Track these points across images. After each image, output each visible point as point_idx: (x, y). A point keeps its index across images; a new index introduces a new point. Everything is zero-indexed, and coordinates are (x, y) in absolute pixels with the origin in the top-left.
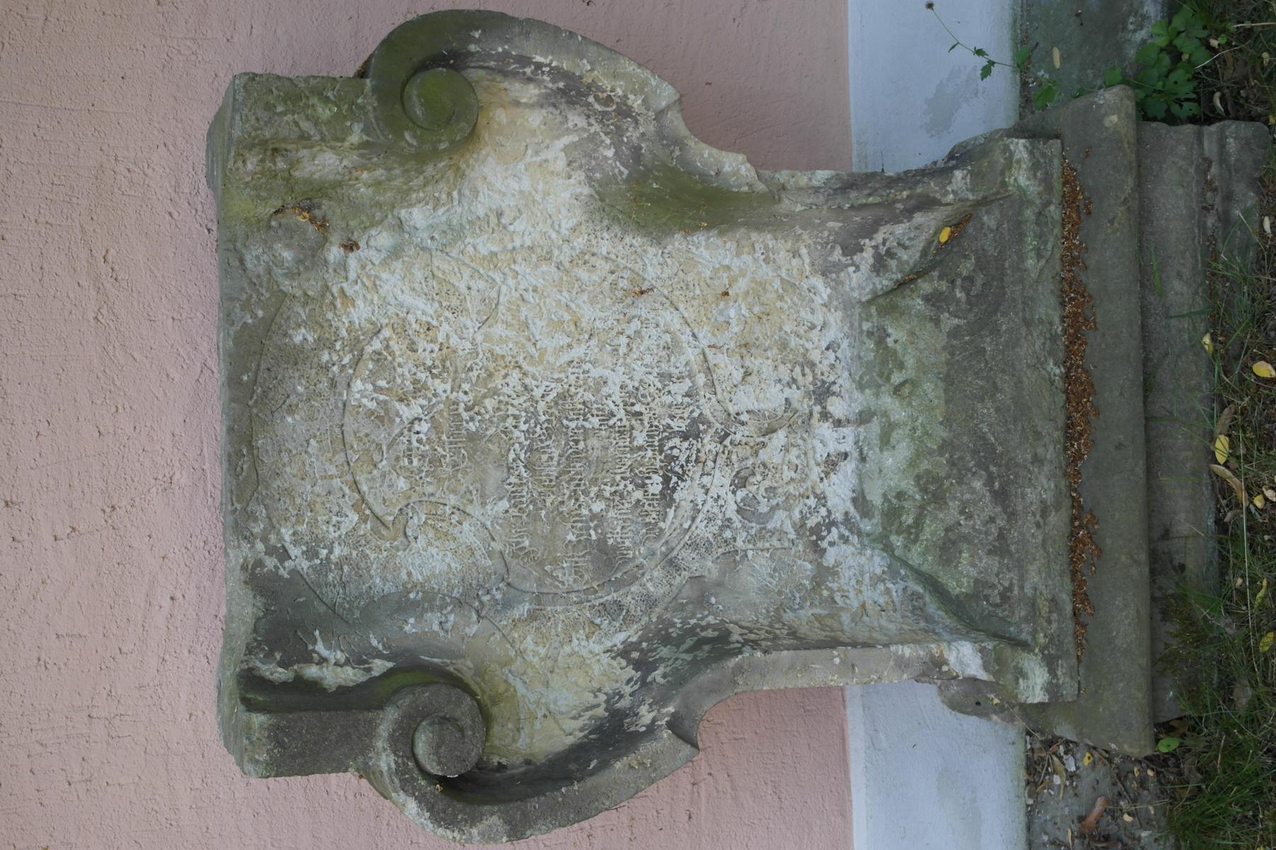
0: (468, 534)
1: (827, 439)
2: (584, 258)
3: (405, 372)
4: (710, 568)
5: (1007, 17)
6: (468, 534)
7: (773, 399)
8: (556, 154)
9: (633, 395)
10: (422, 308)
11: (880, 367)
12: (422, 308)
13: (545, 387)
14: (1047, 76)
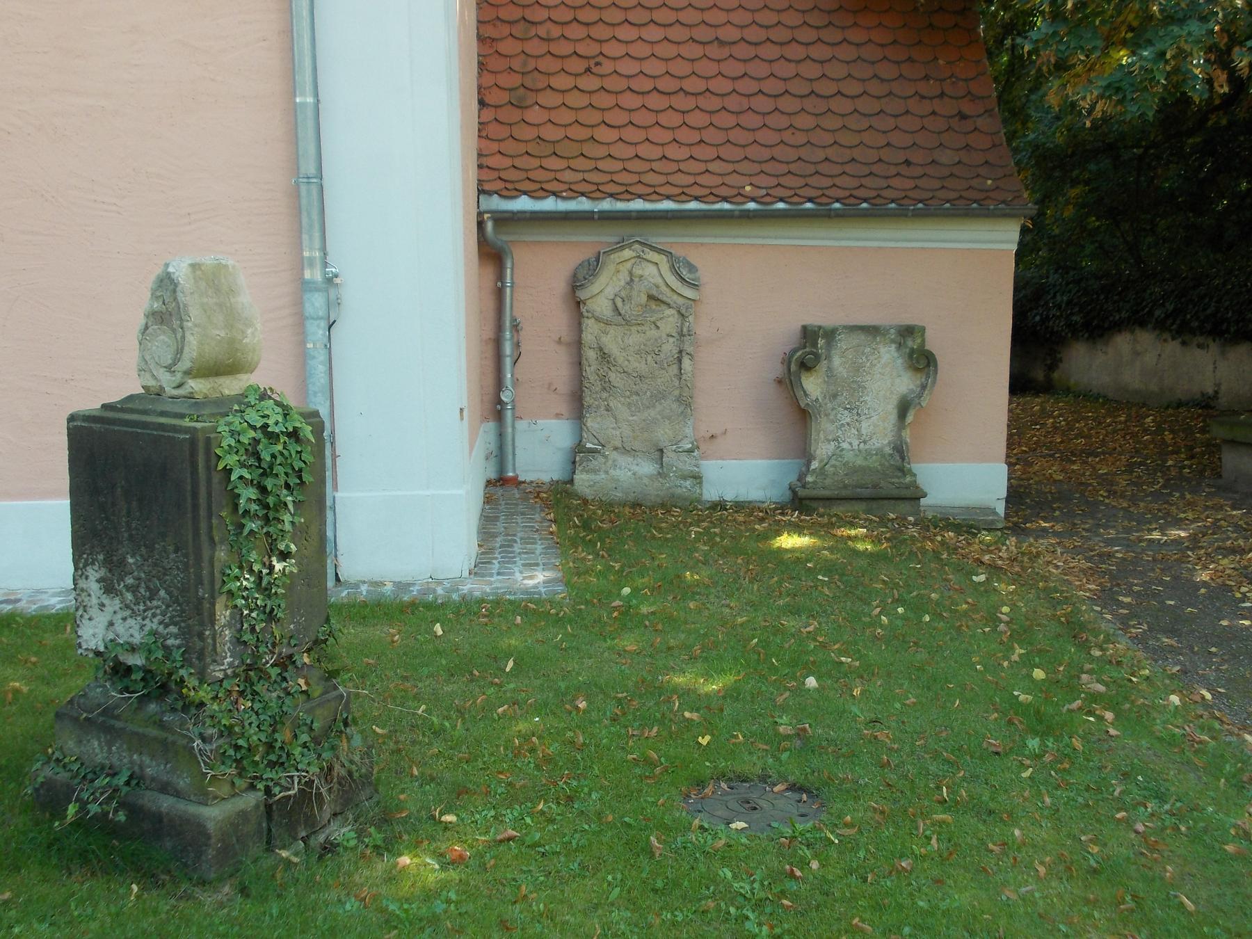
0: (841, 369)
1: (855, 443)
2: (892, 393)
3: (871, 358)
4: (831, 417)
5: (463, 304)
6: (841, 369)
7: (864, 431)
8: (911, 386)
9: (865, 402)
10: (883, 361)
11: (869, 453)
12: (883, 361)
13: (867, 384)
14: (1030, 698)
